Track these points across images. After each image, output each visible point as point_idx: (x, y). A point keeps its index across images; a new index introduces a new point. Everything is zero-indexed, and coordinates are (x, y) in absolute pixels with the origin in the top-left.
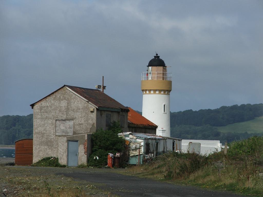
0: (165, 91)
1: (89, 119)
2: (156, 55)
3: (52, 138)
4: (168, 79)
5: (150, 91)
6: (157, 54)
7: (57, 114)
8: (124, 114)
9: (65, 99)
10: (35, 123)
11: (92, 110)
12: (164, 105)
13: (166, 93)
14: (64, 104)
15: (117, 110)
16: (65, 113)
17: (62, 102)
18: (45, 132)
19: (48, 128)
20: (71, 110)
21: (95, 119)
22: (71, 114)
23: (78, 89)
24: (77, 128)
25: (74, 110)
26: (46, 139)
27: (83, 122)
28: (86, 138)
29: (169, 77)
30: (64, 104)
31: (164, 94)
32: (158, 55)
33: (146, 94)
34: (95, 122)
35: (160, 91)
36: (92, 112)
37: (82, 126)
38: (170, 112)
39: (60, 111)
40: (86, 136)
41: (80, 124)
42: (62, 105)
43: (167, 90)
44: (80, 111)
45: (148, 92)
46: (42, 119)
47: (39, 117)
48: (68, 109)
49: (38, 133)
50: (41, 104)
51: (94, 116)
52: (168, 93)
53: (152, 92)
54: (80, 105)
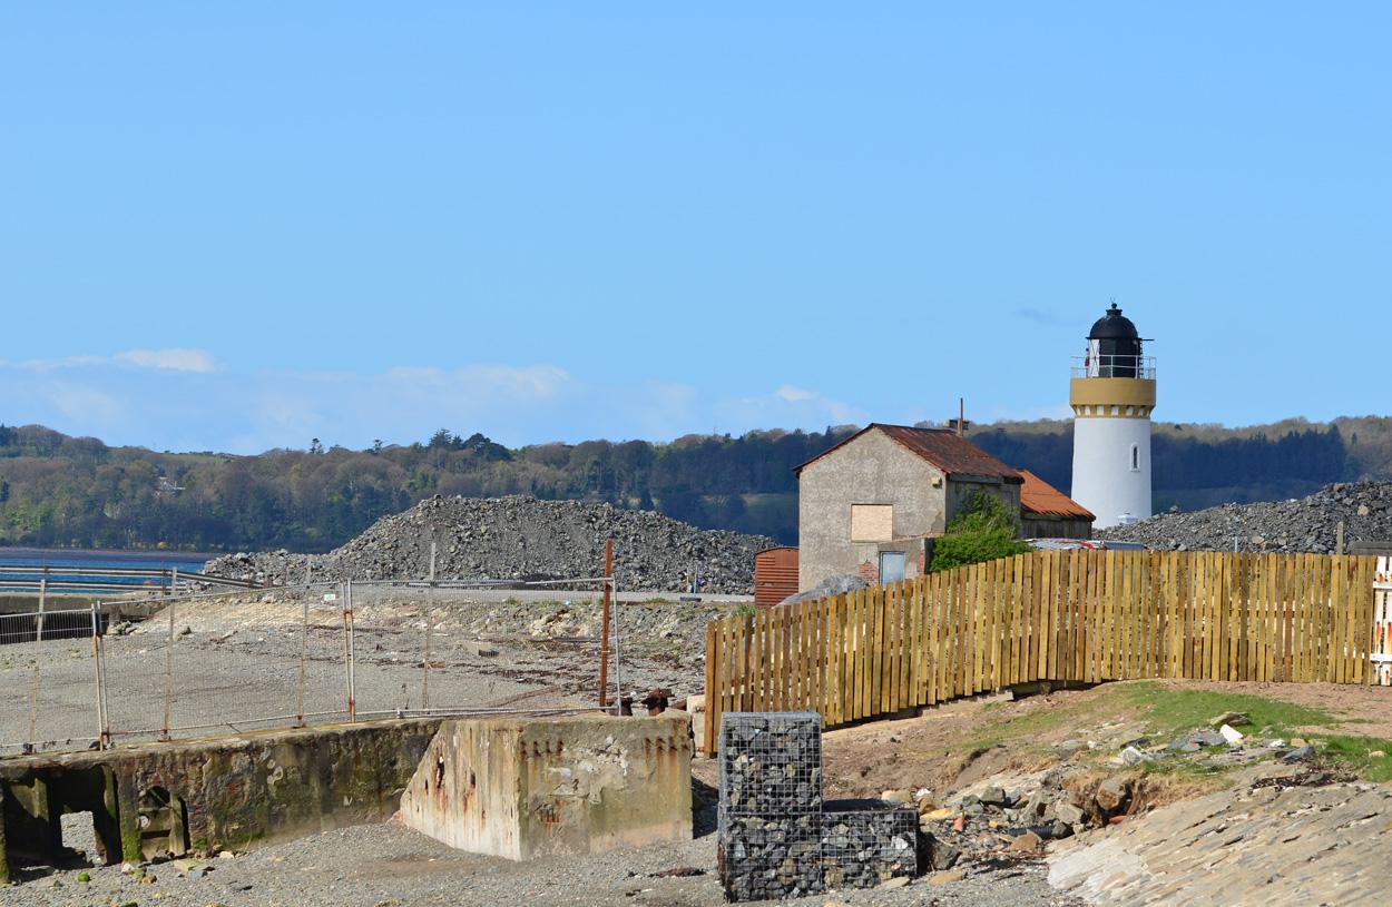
0: (1136, 408)
1: (929, 502)
2: (1111, 308)
3: (843, 545)
4: (1146, 377)
5: (1094, 407)
6: (1114, 306)
7: (854, 491)
8: (1012, 487)
9: (873, 455)
10: (802, 512)
11: (936, 481)
12: (1135, 450)
13: (1141, 413)
14: (870, 467)
15: (993, 481)
16: (873, 488)
17: (867, 462)
18: (826, 532)
19: (834, 522)
20: (888, 482)
21: (944, 503)
22: (888, 490)
23: (903, 430)
24: (902, 522)
25: (894, 481)
26: (830, 547)
27: (915, 508)
28: (923, 548)
29: (1149, 370)
30: (870, 467)
31: (1135, 415)
32: (1118, 308)
33: (1083, 415)
34: (944, 511)
35: (1123, 408)
36: (935, 486)
37: (911, 518)
38: (689, 783)
39: (862, 483)
40: (923, 542)
41: (908, 515)
42: (866, 471)
43: (1143, 406)
44: (908, 483)
45: (1088, 412)
46: (820, 501)
47: (812, 496)
48: (879, 479)
49: (811, 535)
50: (818, 468)
51: (941, 494)
52: (1145, 414)
53: (1100, 412)
54: (908, 471)
